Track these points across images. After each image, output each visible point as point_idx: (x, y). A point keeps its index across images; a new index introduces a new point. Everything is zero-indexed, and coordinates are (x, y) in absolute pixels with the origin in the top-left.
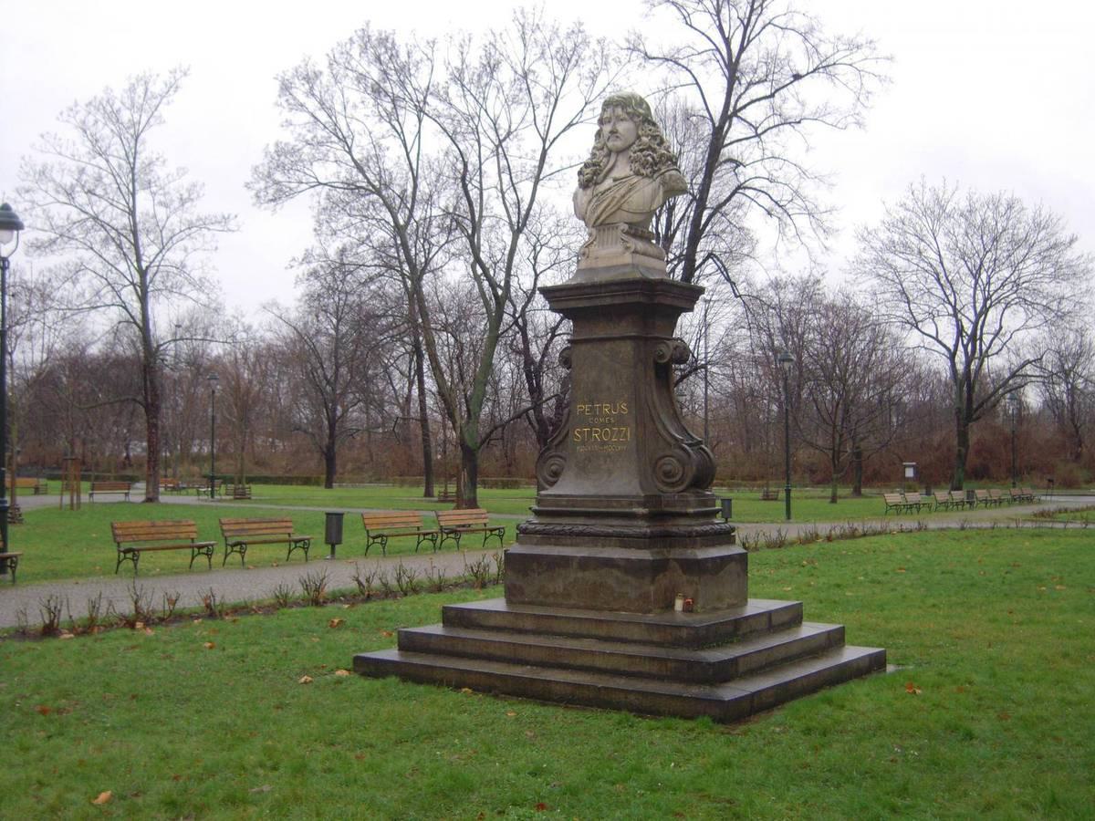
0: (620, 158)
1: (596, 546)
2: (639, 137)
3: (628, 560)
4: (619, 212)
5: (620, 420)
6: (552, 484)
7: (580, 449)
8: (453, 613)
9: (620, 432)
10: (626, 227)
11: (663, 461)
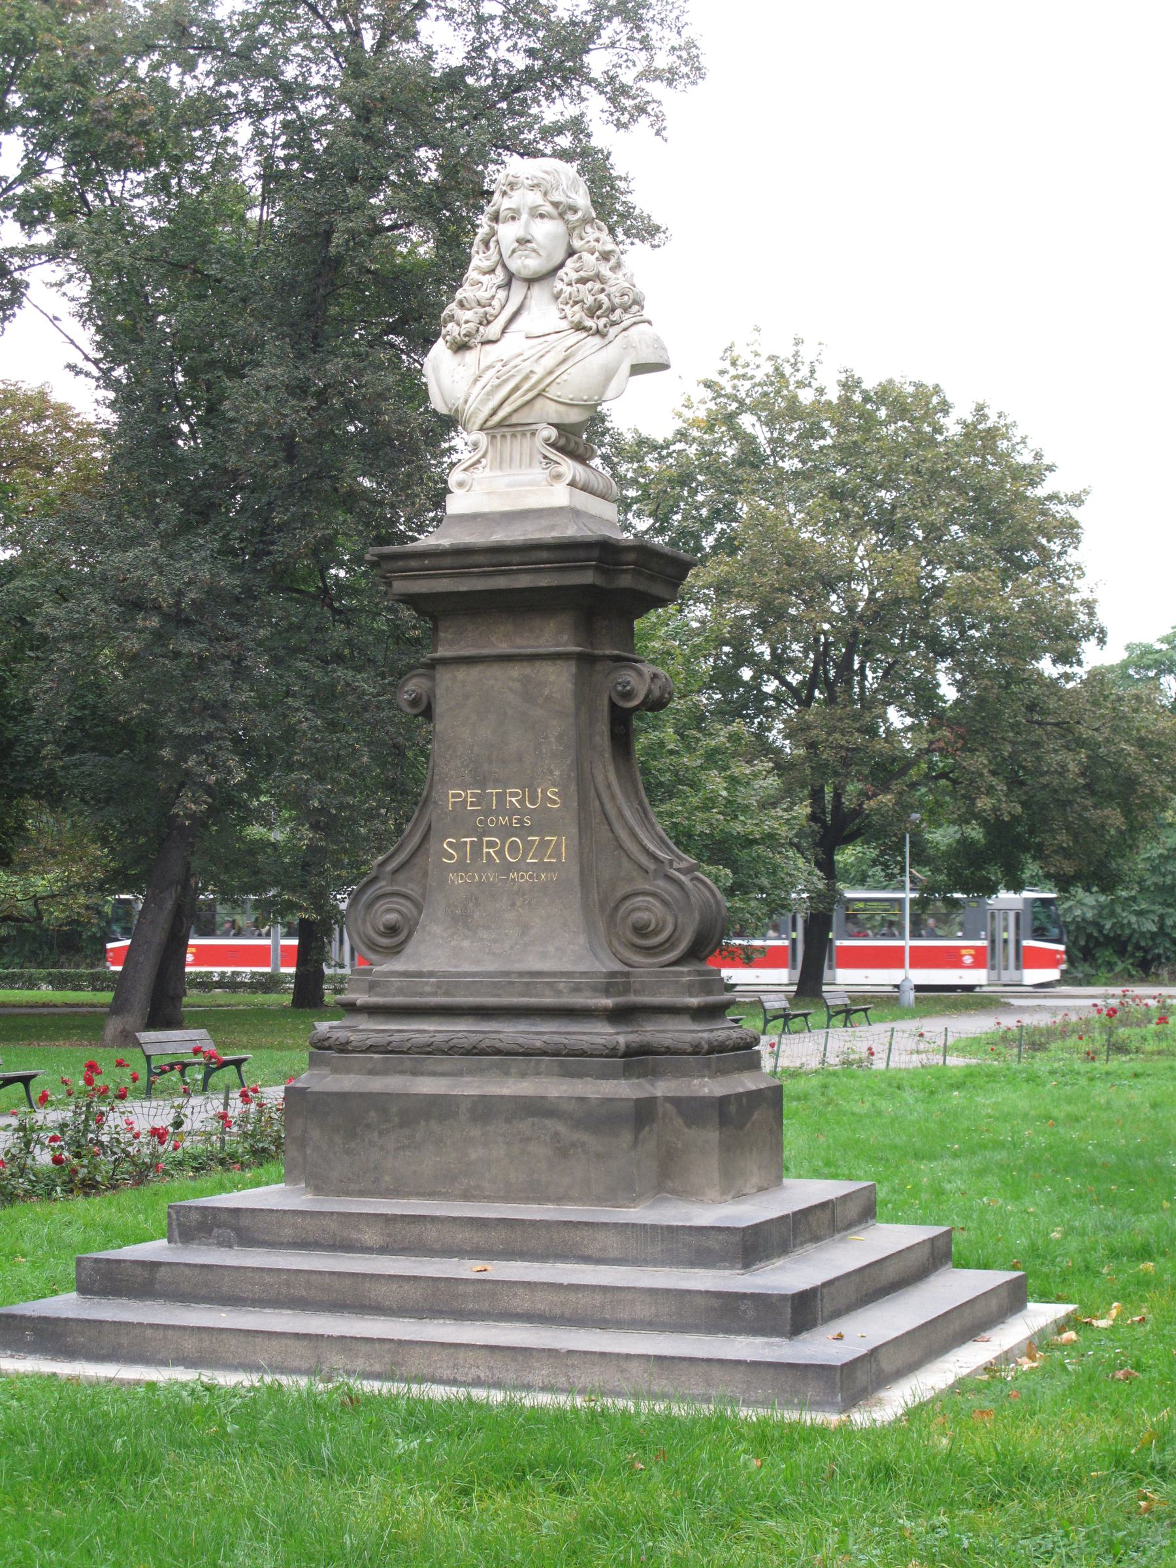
0: (536, 290)
1: (507, 1074)
2: (571, 253)
3: (582, 1099)
4: (539, 403)
5: (544, 823)
6: (395, 951)
8: (195, 1216)
9: (544, 844)
10: (553, 433)
11: (628, 904)
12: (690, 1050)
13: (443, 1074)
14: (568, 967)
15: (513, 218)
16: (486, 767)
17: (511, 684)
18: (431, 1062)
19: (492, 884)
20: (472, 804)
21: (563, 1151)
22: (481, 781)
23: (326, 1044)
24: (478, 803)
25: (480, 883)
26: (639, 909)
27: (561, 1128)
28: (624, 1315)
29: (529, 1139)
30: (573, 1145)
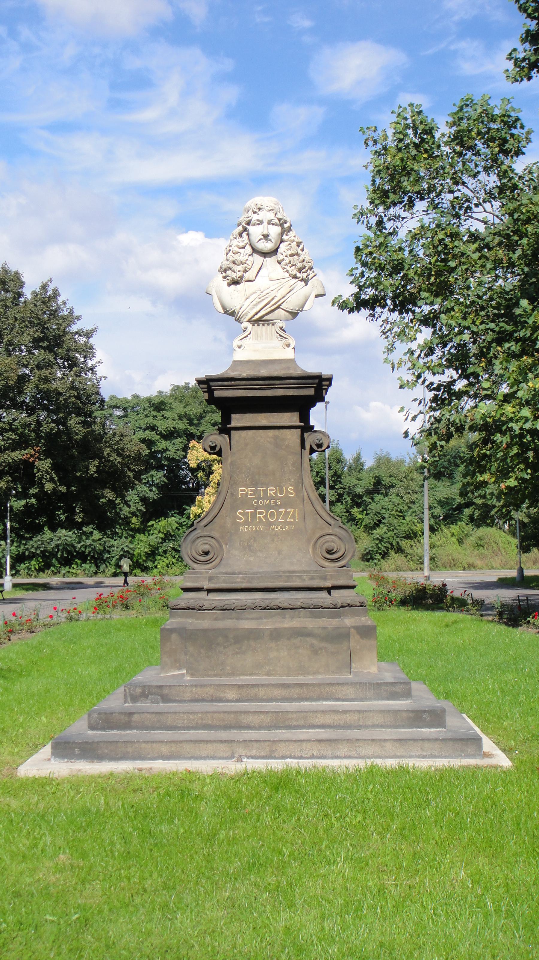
3: (324, 628)
5: (287, 503)
7: (245, 529)
9: (287, 513)
12: (359, 604)
13: (253, 619)
14: (307, 568)
17: (268, 439)
18: (247, 614)
20: (251, 494)
21: (315, 652)
22: (255, 484)
23: (178, 607)
26: (328, 542)
27: (315, 642)
28: (369, 723)
30: (321, 649)
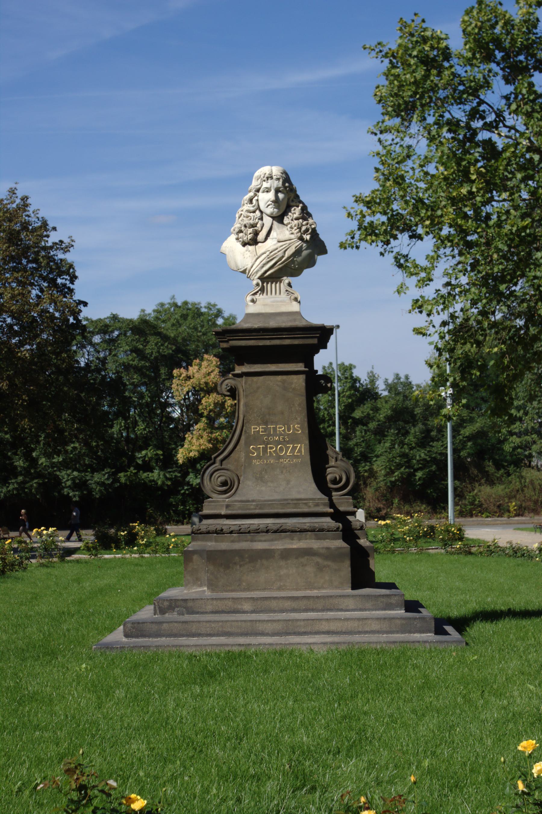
1: (292, 539)
3: (328, 548)
5: (294, 439)
7: (256, 462)
8: (166, 604)
13: (265, 541)
15: (267, 192)
16: (267, 417)
19: (272, 464)
20: (262, 432)
21: (320, 569)
24: (265, 432)
25: (267, 464)
27: (319, 560)
29: (306, 565)
30: (324, 566)
